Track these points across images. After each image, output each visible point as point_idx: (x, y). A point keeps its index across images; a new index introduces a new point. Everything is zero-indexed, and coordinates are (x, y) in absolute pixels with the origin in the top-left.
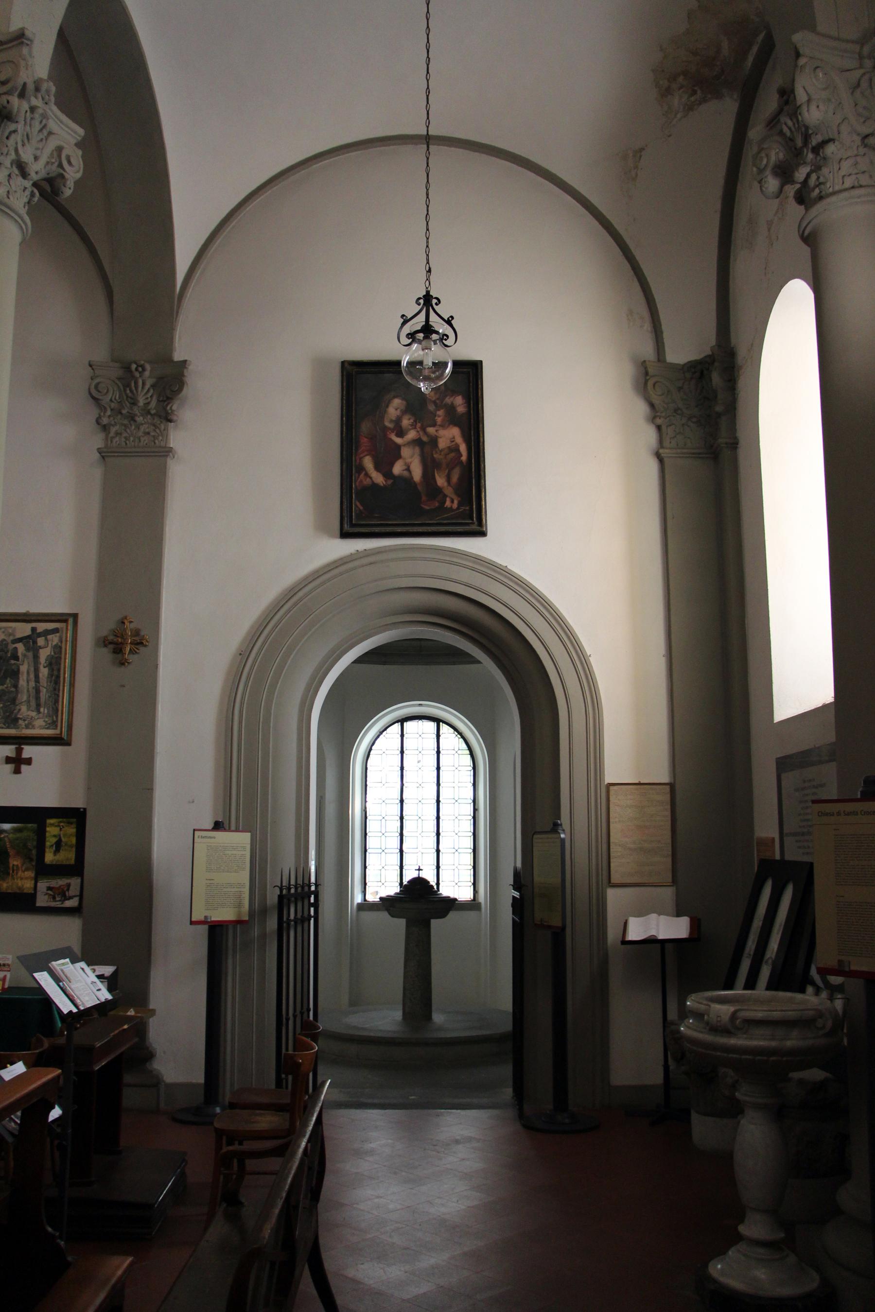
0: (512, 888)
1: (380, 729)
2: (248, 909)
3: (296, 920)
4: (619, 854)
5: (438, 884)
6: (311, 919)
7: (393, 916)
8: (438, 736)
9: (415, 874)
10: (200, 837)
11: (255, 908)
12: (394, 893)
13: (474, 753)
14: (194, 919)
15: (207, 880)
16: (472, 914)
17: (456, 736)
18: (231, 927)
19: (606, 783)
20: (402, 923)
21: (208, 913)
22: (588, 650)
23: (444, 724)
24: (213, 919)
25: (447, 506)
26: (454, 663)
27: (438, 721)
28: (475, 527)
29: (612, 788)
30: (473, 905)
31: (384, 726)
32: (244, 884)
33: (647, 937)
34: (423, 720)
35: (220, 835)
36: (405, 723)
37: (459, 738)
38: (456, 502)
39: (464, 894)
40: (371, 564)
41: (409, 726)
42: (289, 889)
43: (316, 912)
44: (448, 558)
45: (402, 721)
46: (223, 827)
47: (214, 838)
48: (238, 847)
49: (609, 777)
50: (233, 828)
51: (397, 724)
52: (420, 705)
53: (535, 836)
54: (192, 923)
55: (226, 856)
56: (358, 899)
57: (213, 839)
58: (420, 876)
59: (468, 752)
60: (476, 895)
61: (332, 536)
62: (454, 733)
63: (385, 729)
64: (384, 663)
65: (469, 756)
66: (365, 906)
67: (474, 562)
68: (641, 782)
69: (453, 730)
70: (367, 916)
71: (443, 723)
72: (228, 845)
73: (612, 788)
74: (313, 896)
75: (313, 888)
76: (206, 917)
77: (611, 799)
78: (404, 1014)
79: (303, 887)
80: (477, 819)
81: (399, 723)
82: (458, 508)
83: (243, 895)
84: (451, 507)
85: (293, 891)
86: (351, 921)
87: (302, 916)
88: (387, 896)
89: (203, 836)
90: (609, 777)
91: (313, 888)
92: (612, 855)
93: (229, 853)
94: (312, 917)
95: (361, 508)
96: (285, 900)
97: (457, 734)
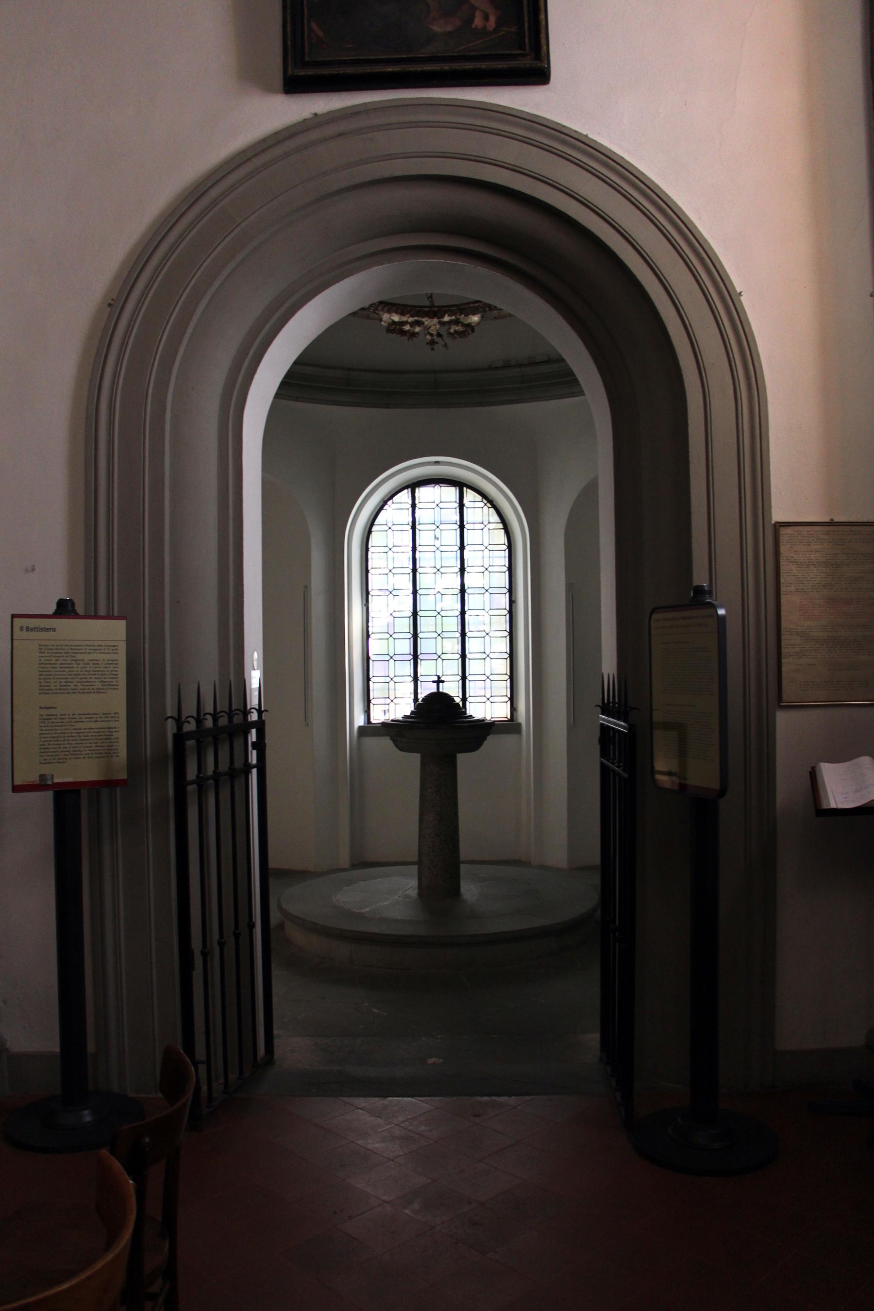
0: (600, 712)
1: (383, 498)
2: (126, 758)
3: (217, 777)
4: (798, 649)
5: (464, 699)
6: (250, 772)
7: (401, 750)
8: (461, 506)
9: (433, 688)
10: (25, 628)
11: (146, 758)
12: (402, 716)
13: (509, 528)
14: (18, 782)
15: (41, 708)
16: (508, 739)
17: (485, 504)
18: (84, 793)
19: (773, 522)
20: (415, 758)
21: (46, 770)
22: (738, 283)
23: (468, 490)
24: (56, 780)
25: (476, 26)
26: (481, 404)
27: (460, 485)
28: (527, 62)
29: (783, 531)
30: (510, 726)
31: (390, 492)
32: (117, 713)
33: (867, 803)
34: (441, 485)
35: (67, 626)
36: (417, 490)
37: (489, 508)
38: (492, 19)
39: (499, 711)
40: (340, 135)
41: (424, 493)
42: (199, 721)
43: (261, 757)
44: (479, 122)
45: (413, 486)
46: (74, 611)
47: (54, 630)
48: (101, 646)
49: (778, 515)
50: (102, 612)
51: (406, 490)
52: (437, 463)
53: (655, 616)
54: (16, 789)
55: (79, 664)
56: (360, 720)
57: (52, 633)
58: (441, 690)
59: (501, 526)
60: (515, 713)
61: (269, 89)
62: (482, 501)
63: (391, 498)
64: (387, 406)
65: (503, 531)
66: (369, 730)
67: (527, 128)
68: (836, 520)
69: (481, 498)
70: (370, 742)
71: (467, 488)
72: (66, 643)
73: (783, 531)
74: (254, 731)
75: (254, 717)
76: (42, 777)
77: (783, 549)
78: (420, 887)
79: (231, 715)
80: (514, 614)
81: (410, 490)
82: (497, 29)
83: (116, 735)
84: (485, 27)
85: (209, 723)
86: (350, 749)
87: (214, 772)
88: (392, 720)
89: (31, 626)
90: (778, 515)
91: (254, 717)
92: (784, 651)
93: (86, 657)
94: (254, 767)
95: (321, 34)
96: (191, 743)
97: (486, 502)
